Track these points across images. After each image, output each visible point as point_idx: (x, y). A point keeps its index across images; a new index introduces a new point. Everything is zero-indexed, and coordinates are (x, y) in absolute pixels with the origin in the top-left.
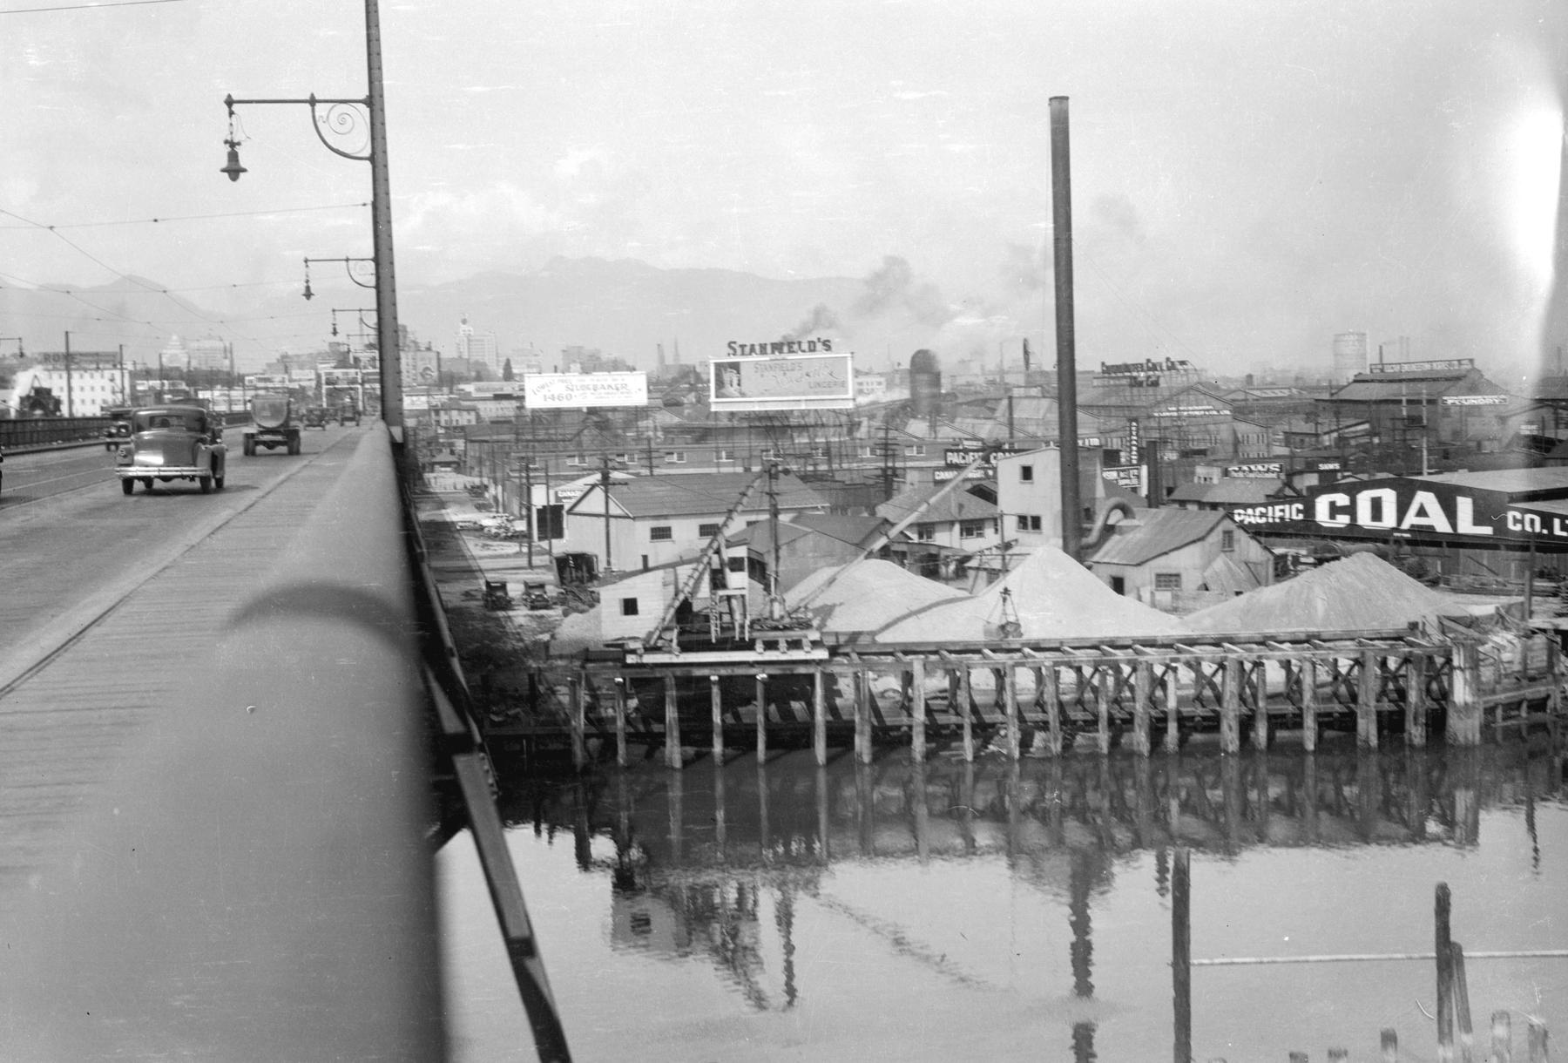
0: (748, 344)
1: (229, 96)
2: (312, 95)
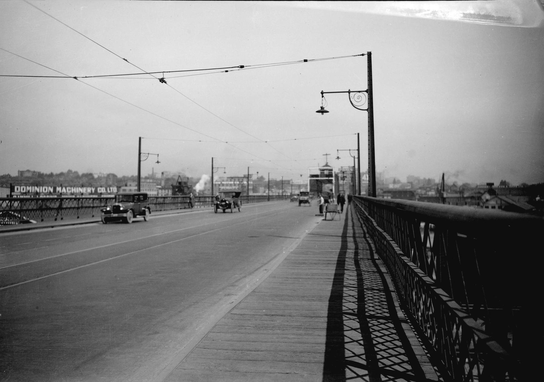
0: (309, 179)
1: (322, 91)
2: (349, 90)
